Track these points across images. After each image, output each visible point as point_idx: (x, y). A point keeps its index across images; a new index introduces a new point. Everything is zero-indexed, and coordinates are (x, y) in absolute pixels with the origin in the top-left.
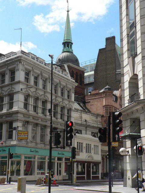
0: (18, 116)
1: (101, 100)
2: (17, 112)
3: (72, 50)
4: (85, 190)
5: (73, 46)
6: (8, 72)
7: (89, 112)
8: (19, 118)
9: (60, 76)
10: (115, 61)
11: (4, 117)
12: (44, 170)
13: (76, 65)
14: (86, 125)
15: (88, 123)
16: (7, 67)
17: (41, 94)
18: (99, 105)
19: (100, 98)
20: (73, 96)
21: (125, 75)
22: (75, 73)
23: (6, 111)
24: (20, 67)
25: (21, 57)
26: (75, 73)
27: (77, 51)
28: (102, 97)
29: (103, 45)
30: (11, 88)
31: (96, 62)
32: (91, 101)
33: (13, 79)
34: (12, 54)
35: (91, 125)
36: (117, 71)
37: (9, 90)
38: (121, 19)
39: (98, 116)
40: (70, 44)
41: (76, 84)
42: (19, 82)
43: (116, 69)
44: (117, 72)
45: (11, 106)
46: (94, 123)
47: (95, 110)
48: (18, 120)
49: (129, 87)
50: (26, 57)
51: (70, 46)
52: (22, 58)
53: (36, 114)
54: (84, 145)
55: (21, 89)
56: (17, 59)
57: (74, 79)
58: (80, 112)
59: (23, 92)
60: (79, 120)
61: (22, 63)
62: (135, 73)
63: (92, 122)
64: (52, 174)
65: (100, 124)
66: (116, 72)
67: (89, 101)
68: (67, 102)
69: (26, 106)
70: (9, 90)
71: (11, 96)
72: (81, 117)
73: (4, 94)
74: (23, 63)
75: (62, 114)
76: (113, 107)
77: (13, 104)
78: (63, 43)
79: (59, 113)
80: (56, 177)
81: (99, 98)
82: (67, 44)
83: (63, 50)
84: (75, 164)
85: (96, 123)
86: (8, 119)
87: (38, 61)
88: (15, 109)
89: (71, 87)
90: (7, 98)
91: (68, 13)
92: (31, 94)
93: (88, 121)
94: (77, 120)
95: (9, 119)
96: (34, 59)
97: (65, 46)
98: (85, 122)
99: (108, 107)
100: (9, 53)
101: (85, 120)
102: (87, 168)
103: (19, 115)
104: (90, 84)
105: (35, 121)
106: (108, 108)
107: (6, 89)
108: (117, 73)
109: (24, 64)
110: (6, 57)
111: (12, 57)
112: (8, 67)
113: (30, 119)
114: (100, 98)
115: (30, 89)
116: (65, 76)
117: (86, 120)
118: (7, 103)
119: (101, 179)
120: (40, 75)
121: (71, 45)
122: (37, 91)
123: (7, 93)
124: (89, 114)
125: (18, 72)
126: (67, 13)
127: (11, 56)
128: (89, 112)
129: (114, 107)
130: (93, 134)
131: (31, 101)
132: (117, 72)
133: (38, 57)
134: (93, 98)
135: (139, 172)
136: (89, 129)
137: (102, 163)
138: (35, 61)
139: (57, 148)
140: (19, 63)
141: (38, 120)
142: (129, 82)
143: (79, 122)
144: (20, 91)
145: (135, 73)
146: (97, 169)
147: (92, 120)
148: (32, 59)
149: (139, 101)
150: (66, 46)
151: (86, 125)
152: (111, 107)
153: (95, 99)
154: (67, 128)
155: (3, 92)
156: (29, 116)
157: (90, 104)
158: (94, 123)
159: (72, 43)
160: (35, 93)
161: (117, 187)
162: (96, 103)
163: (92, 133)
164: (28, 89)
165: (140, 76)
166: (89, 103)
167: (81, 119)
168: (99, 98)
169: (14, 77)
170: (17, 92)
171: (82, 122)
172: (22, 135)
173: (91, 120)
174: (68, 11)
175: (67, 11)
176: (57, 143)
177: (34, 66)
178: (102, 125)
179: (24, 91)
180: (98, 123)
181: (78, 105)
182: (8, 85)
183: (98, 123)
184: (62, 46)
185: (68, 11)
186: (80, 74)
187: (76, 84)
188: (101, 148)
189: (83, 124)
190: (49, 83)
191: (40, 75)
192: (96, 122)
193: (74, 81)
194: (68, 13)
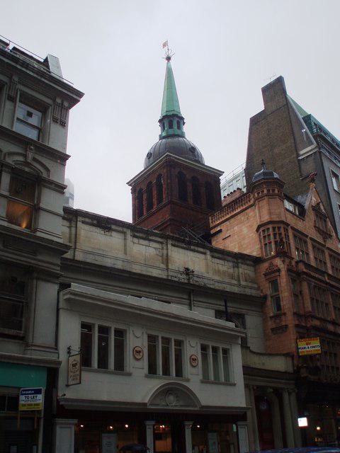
10: (293, 131)
18: (245, 230)
27: (193, 134)
29: (259, 106)
32: (222, 227)
36: (301, 152)
43: (297, 150)
44: (302, 155)
63: (217, 278)
66: (298, 155)
67: (218, 229)
72: (166, 260)
76: (290, 230)
82: (172, 121)
85: (236, 282)
98: (184, 276)
99: (270, 226)
102: (43, 443)
106: (271, 230)
108: (300, 158)
117: (187, 269)
129: (292, 228)
132: (302, 155)
134: (228, 216)
135: (20, 213)
136: (201, 300)
137: (252, 417)
147: (218, 272)
152: (282, 226)
153: (232, 217)
157: (222, 236)
162: (236, 228)
167: (167, 266)
171: (171, 273)
174: (168, 59)
180: (243, 283)
185: (168, 59)
188: (243, 360)
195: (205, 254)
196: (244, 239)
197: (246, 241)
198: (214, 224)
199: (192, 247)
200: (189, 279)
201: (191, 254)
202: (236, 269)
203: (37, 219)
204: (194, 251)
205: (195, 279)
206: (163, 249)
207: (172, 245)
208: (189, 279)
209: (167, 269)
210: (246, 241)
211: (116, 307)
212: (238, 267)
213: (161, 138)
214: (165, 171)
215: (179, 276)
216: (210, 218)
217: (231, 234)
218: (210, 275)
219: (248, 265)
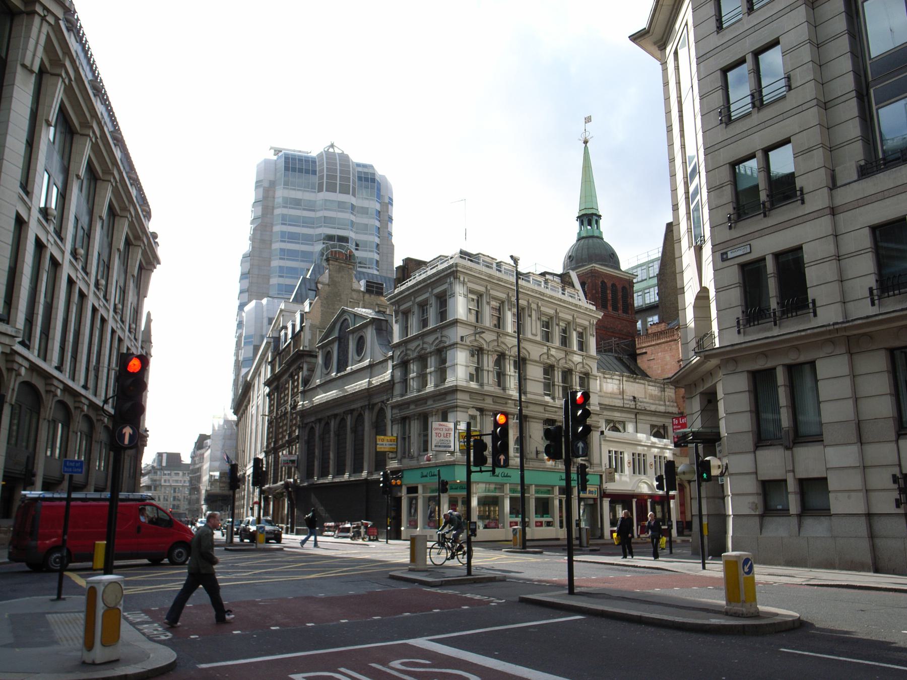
0: (457, 399)
1: (674, 346)
2: (454, 390)
3: (601, 233)
4: (613, 564)
5: (601, 222)
6: (433, 301)
7: (644, 375)
8: (459, 403)
9: (555, 299)
11: (430, 402)
12: (553, 517)
13: (611, 267)
14: (636, 408)
15: (641, 404)
16: (430, 290)
17: (510, 346)
18: (668, 358)
19: (670, 341)
20: (592, 342)
21: (686, 289)
22: (609, 285)
23: (432, 389)
24: (459, 290)
25: (456, 265)
26: (609, 285)
28: (675, 340)
30: (440, 337)
31: (660, 255)
32: (649, 350)
33: (443, 314)
34: (441, 259)
35: (648, 409)
37: (437, 341)
38: (671, 158)
39: (666, 386)
40: (595, 218)
41: (600, 315)
42: (456, 322)
45: (442, 373)
46: (657, 402)
47: (659, 372)
48: (457, 407)
49: (694, 318)
50: (469, 264)
51: (594, 222)
52: (459, 269)
53: (502, 391)
54: (627, 458)
55: (462, 338)
56: (449, 271)
57: (592, 304)
58: (618, 378)
59: (465, 343)
60: (618, 399)
61: (459, 279)
62: (703, 286)
63: (651, 401)
64: (471, 527)
65: (672, 404)
67: (644, 351)
68: (577, 359)
69: (477, 375)
70: (437, 341)
71: (441, 353)
73: (428, 350)
74: (462, 279)
75: (567, 387)
77: (446, 371)
78: (578, 217)
79: (559, 386)
80: (533, 532)
81: (667, 342)
82: (589, 218)
83: (579, 234)
84: (606, 503)
85: (662, 403)
86: (420, 409)
87: (500, 271)
88: (450, 382)
89: (587, 323)
90: (433, 358)
91: (586, 146)
92: (485, 346)
93: (640, 399)
94: (611, 398)
95: (441, 404)
96: (491, 268)
97: (582, 223)
98: (633, 403)
100: (434, 259)
101: (632, 398)
103: (460, 396)
104: (650, 309)
105: (498, 407)
107: (430, 339)
109: (466, 280)
110: (429, 268)
111: (441, 267)
112: (432, 290)
113: (487, 404)
114: (670, 341)
115: (483, 335)
116: (570, 300)
117: (634, 398)
118: (434, 371)
119: (676, 535)
120: (506, 303)
121: (597, 222)
122: (499, 339)
123: (433, 348)
124: (642, 381)
125: (452, 299)
126: (584, 145)
127: (437, 266)
128: (644, 375)
130: (655, 430)
131: (489, 362)
133: (501, 262)
134: (653, 343)
138: (493, 272)
139: (481, 471)
140: (455, 279)
141: (506, 403)
142: (694, 307)
143: (618, 403)
144: (460, 342)
145: (703, 286)
146: (667, 511)
147: (651, 396)
148: (485, 269)
149: (707, 353)
150: (586, 222)
151: (636, 408)
153: (657, 344)
154: (496, 428)
155: (425, 346)
156: (483, 395)
157: (645, 357)
158: (657, 402)
159: (600, 216)
160: (496, 344)
161: (5, 553)
162: (660, 354)
163: (653, 426)
164: (477, 336)
165: (712, 294)
166: (644, 356)
168: (667, 342)
169: (446, 310)
170: (454, 345)
171: (625, 402)
172: (384, 443)
173: (648, 396)
174: (586, 142)
175: (584, 143)
176: (480, 461)
177: (490, 281)
178: (678, 406)
179: (468, 341)
180: (667, 403)
181: (615, 361)
182: (434, 331)
183: (667, 403)
184: (577, 224)
185: (586, 142)
186: (624, 288)
187: (600, 315)
189: (628, 406)
190: (529, 318)
191: (506, 303)
192: (660, 400)
193: (594, 308)
194: (586, 146)
195: (644, 384)
196: (666, 364)
197: (668, 367)
198: (640, 346)
199: (637, 380)
200: (636, 405)
201: (636, 385)
202: (663, 393)
203: (525, 371)
204: (638, 383)
205: (639, 404)
206: (620, 384)
207: (626, 381)
208: (636, 405)
209: (623, 398)
210: (668, 367)
211: (54, 106)
212: (664, 391)
213: (580, 239)
214: (589, 280)
215: (630, 403)
216: (636, 339)
217: (655, 358)
218: (647, 400)
219: (670, 388)
